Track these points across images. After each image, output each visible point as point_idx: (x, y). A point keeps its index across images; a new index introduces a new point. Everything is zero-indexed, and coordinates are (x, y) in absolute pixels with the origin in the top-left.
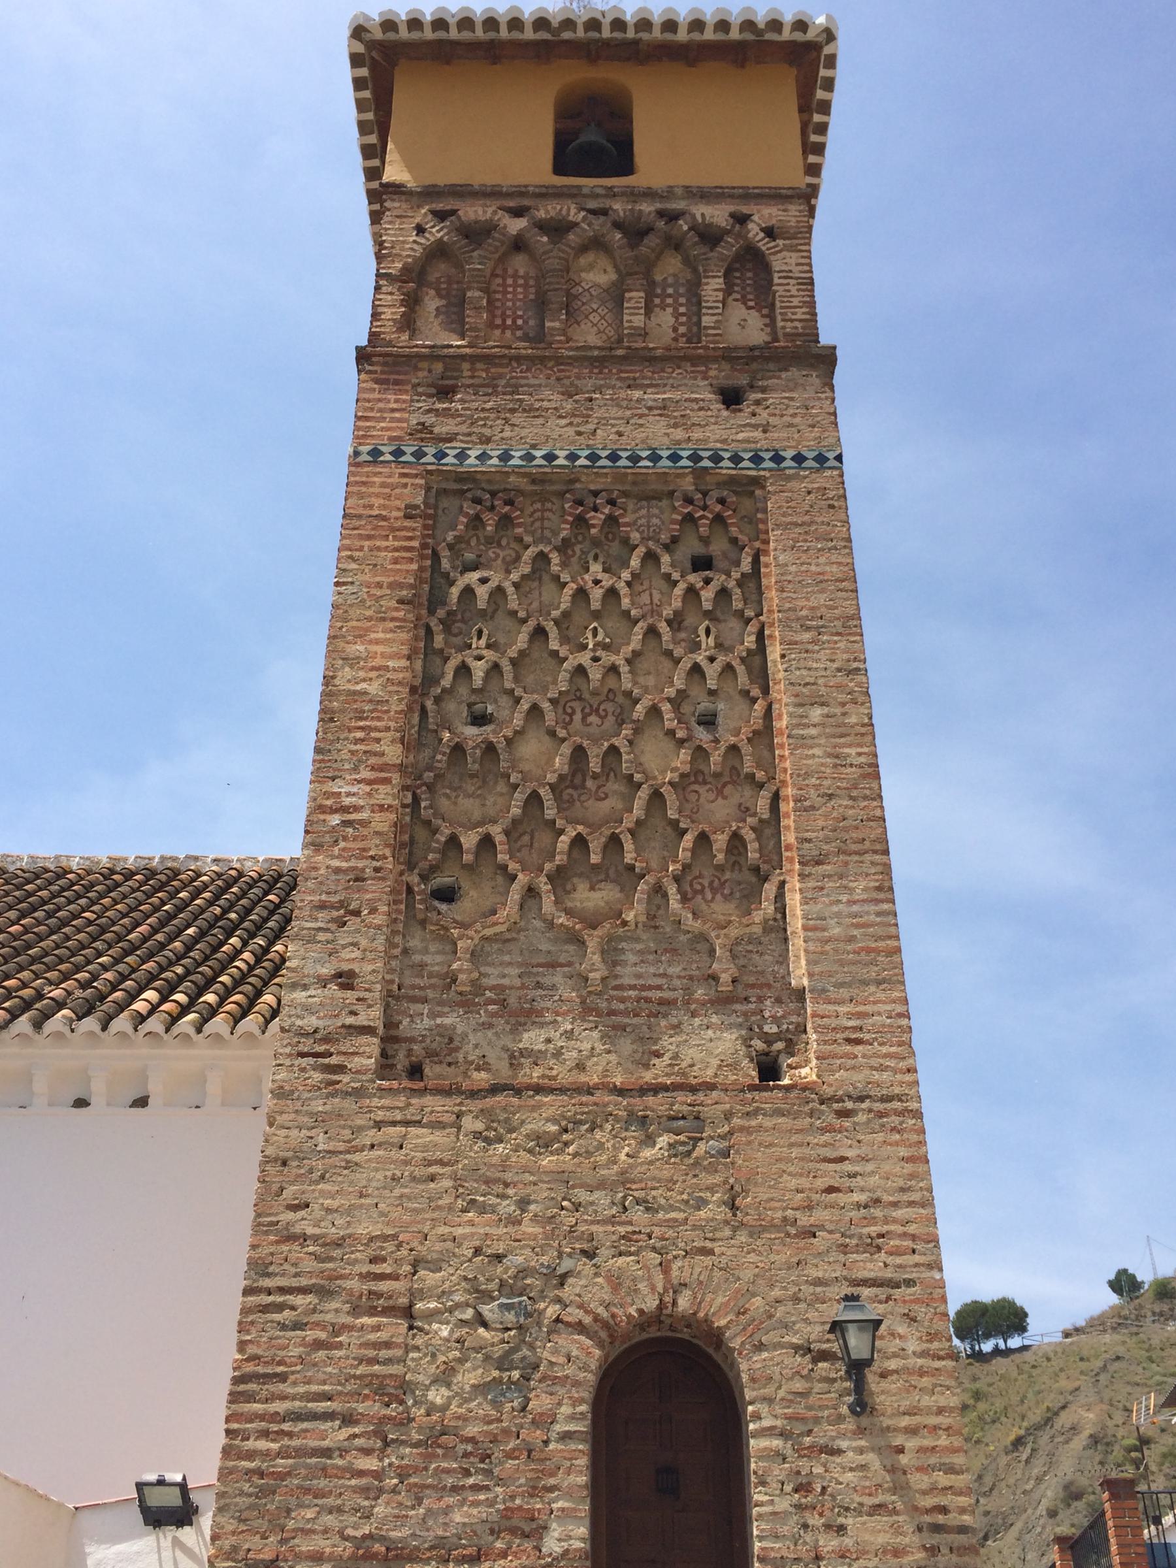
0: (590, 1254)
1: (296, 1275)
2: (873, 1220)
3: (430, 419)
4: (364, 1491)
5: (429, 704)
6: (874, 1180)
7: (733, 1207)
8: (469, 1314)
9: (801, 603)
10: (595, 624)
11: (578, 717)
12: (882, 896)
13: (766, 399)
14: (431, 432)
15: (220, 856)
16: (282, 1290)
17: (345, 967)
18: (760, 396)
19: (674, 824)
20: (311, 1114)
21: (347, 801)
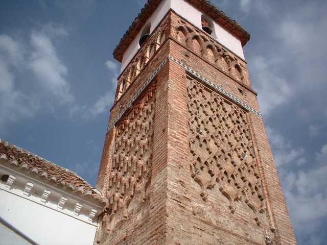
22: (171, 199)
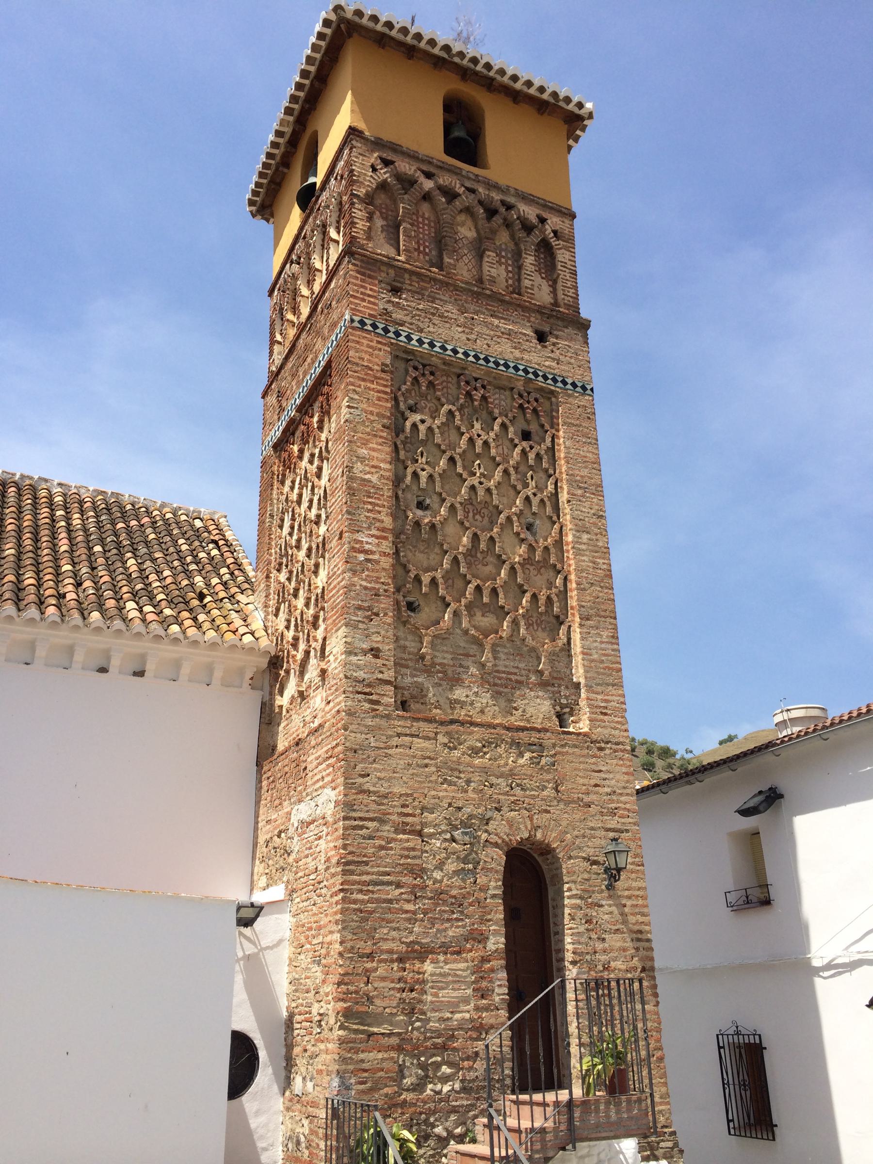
0: (498, 810)
1: (368, 811)
2: (613, 801)
3: (390, 308)
4: (409, 920)
5: (400, 493)
6: (613, 782)
7: (557, 791)
8: (448, 836)
9: (577, 472)
10: (478, 462)
11: (471, 514)
12: (614, 641)
13: (558, 344)
14: (391, 317)
15: (63, 482)
16: (361, 819)
17: (375, 645)
18: (555, 340)
19: (521, 586)
20: (366, 726)
21: (367, 547)
22: (352, 692)
